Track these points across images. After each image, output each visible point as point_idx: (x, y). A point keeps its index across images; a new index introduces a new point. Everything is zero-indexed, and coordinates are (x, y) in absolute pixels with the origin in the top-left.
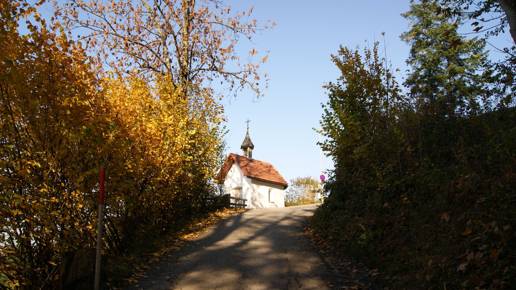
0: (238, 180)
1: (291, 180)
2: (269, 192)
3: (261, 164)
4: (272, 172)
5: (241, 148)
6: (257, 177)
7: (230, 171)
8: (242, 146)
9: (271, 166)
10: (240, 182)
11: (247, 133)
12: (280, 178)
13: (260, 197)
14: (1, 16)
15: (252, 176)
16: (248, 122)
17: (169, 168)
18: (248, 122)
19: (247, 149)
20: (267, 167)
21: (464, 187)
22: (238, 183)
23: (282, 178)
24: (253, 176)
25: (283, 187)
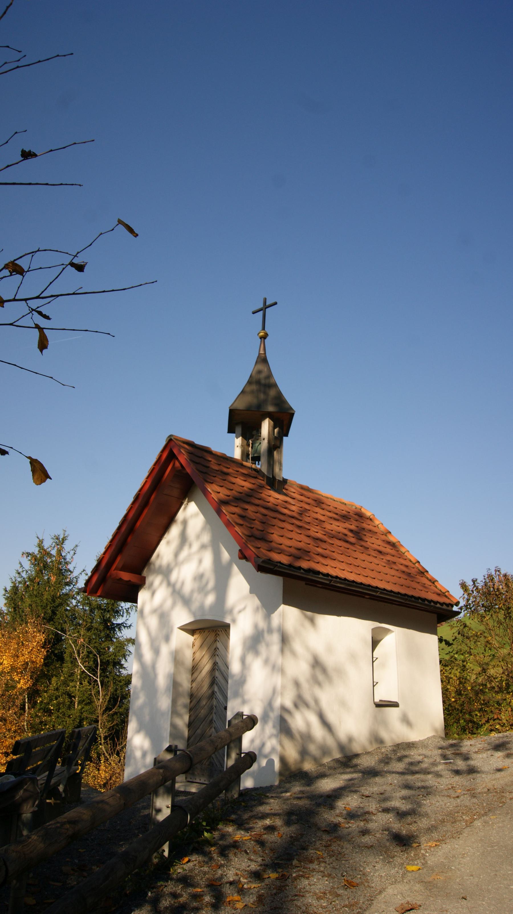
0: (202, 590)
1: (463, 586)
2: (375, 643)
3: (319, 502)
4: (371, 541)
5: (231, 430)
6: (305, 565)
7: (163, 543)
8: (233, 413)
9: (360, 516)
10: (210, 599)
11: (263, 360)
12: (413, 571)
13: (321, 677)
14: (5, 609)
15: (276, 557)
16: (265, 307)
17: (3, 677)
18: (265, 307)
19: (258, 428)
20: (345, 517)
21: (331, 865)
22: (202, 607)
23: (423, 572)
24: (285, 559)
25: (435, 616)
